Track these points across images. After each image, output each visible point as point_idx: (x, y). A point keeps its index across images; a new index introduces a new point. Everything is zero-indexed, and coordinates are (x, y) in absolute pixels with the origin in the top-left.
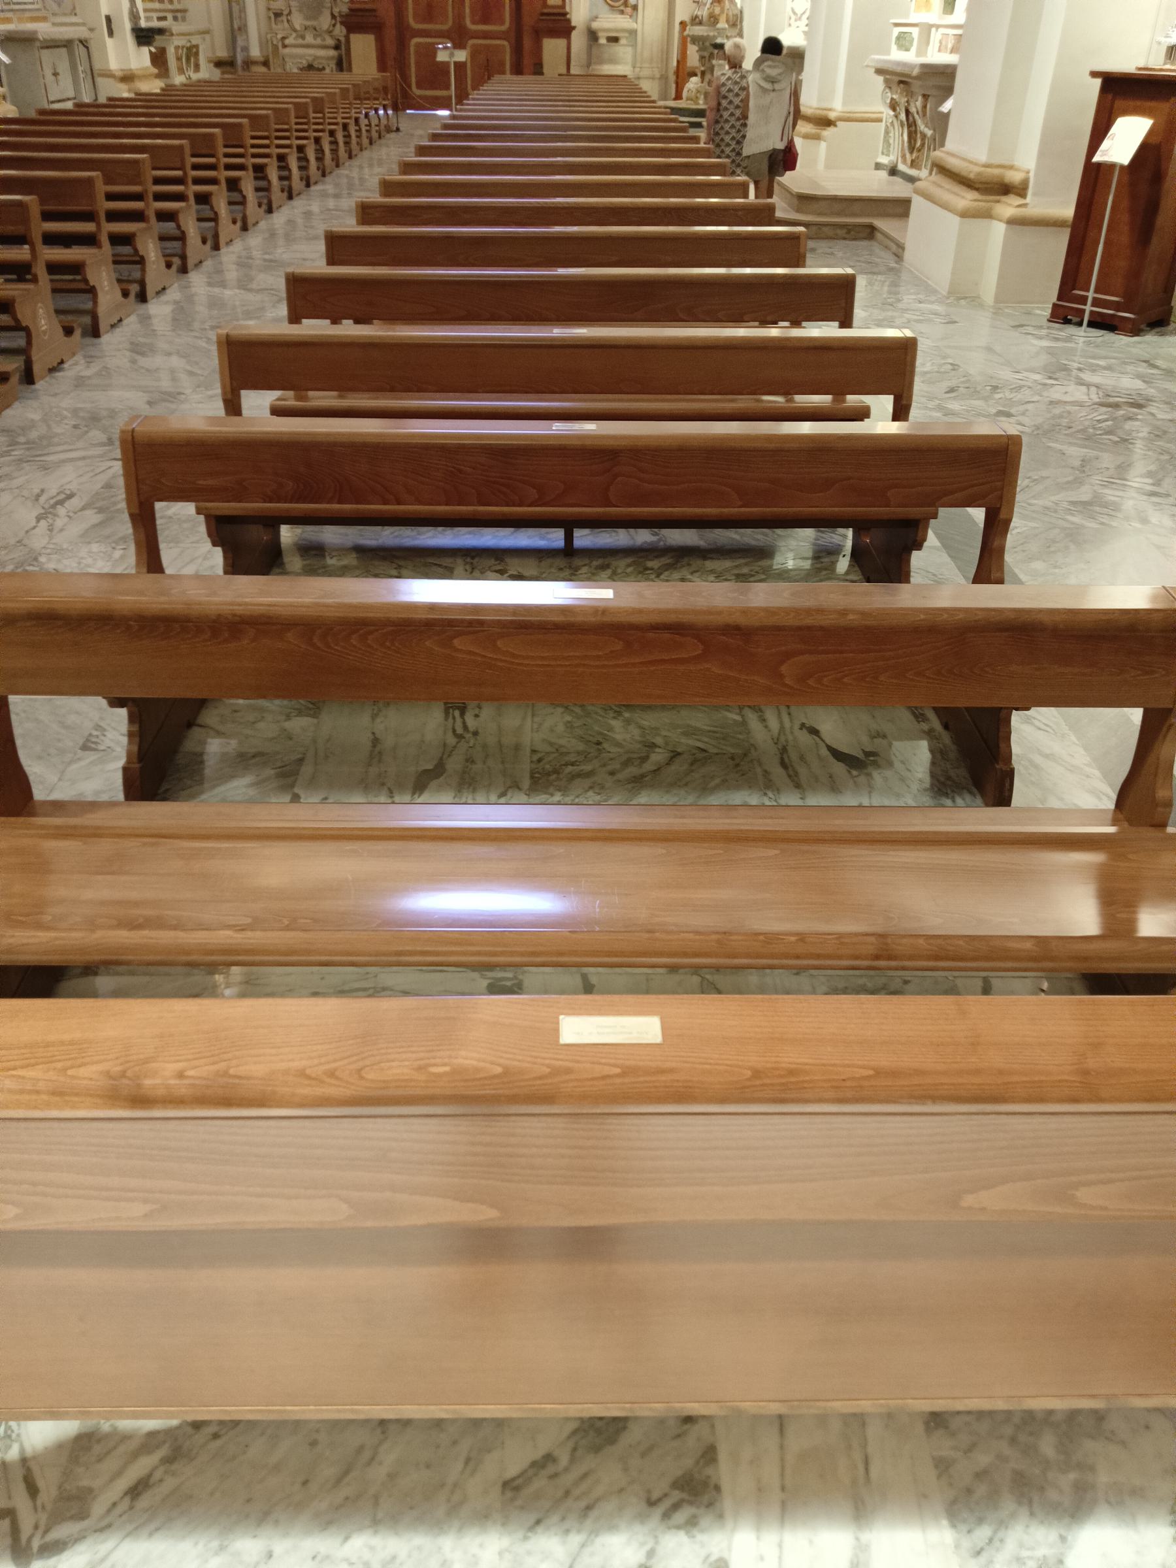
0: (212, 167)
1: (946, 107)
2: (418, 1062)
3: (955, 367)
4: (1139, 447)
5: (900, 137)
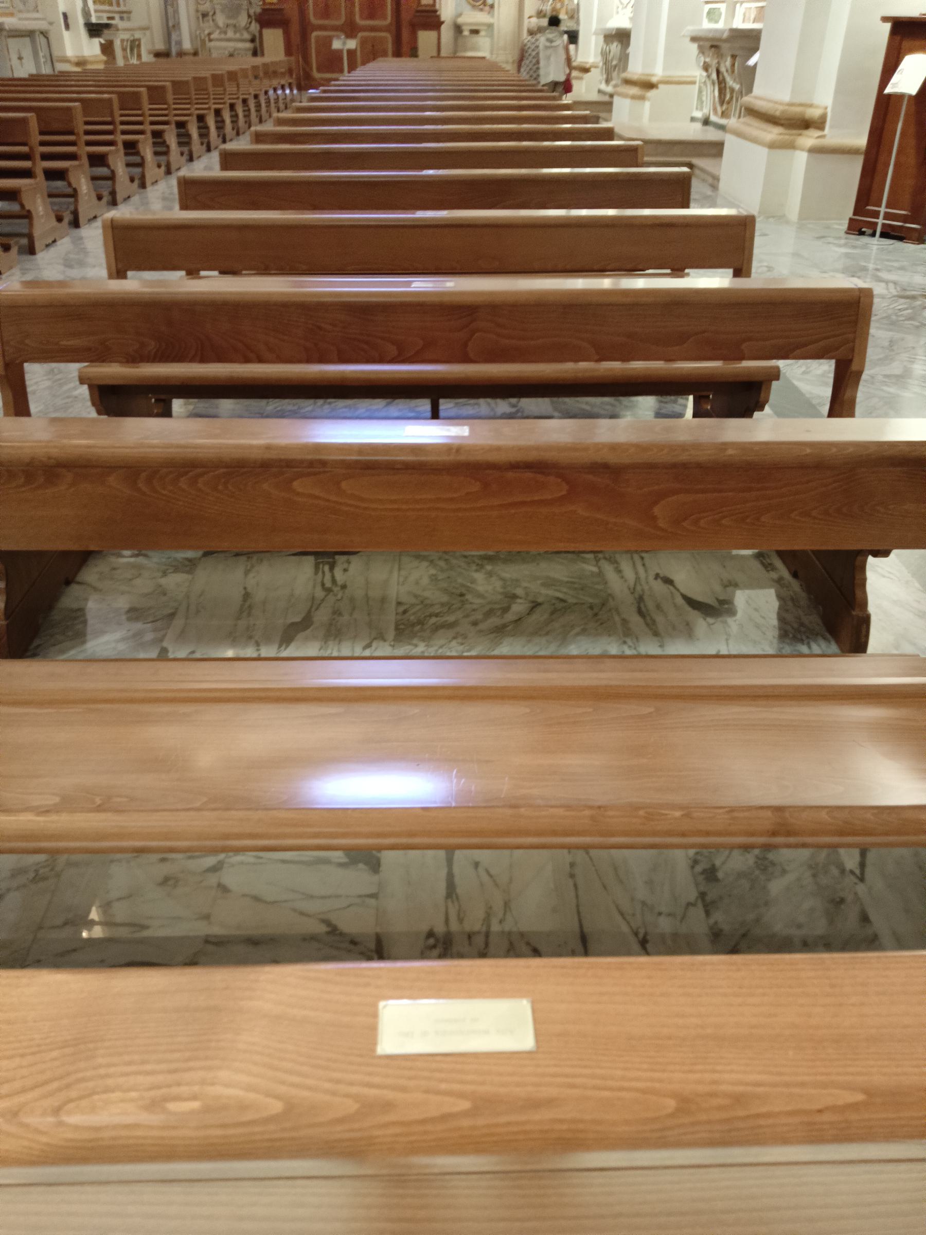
1: (751, 62)
2: (152, 1093)
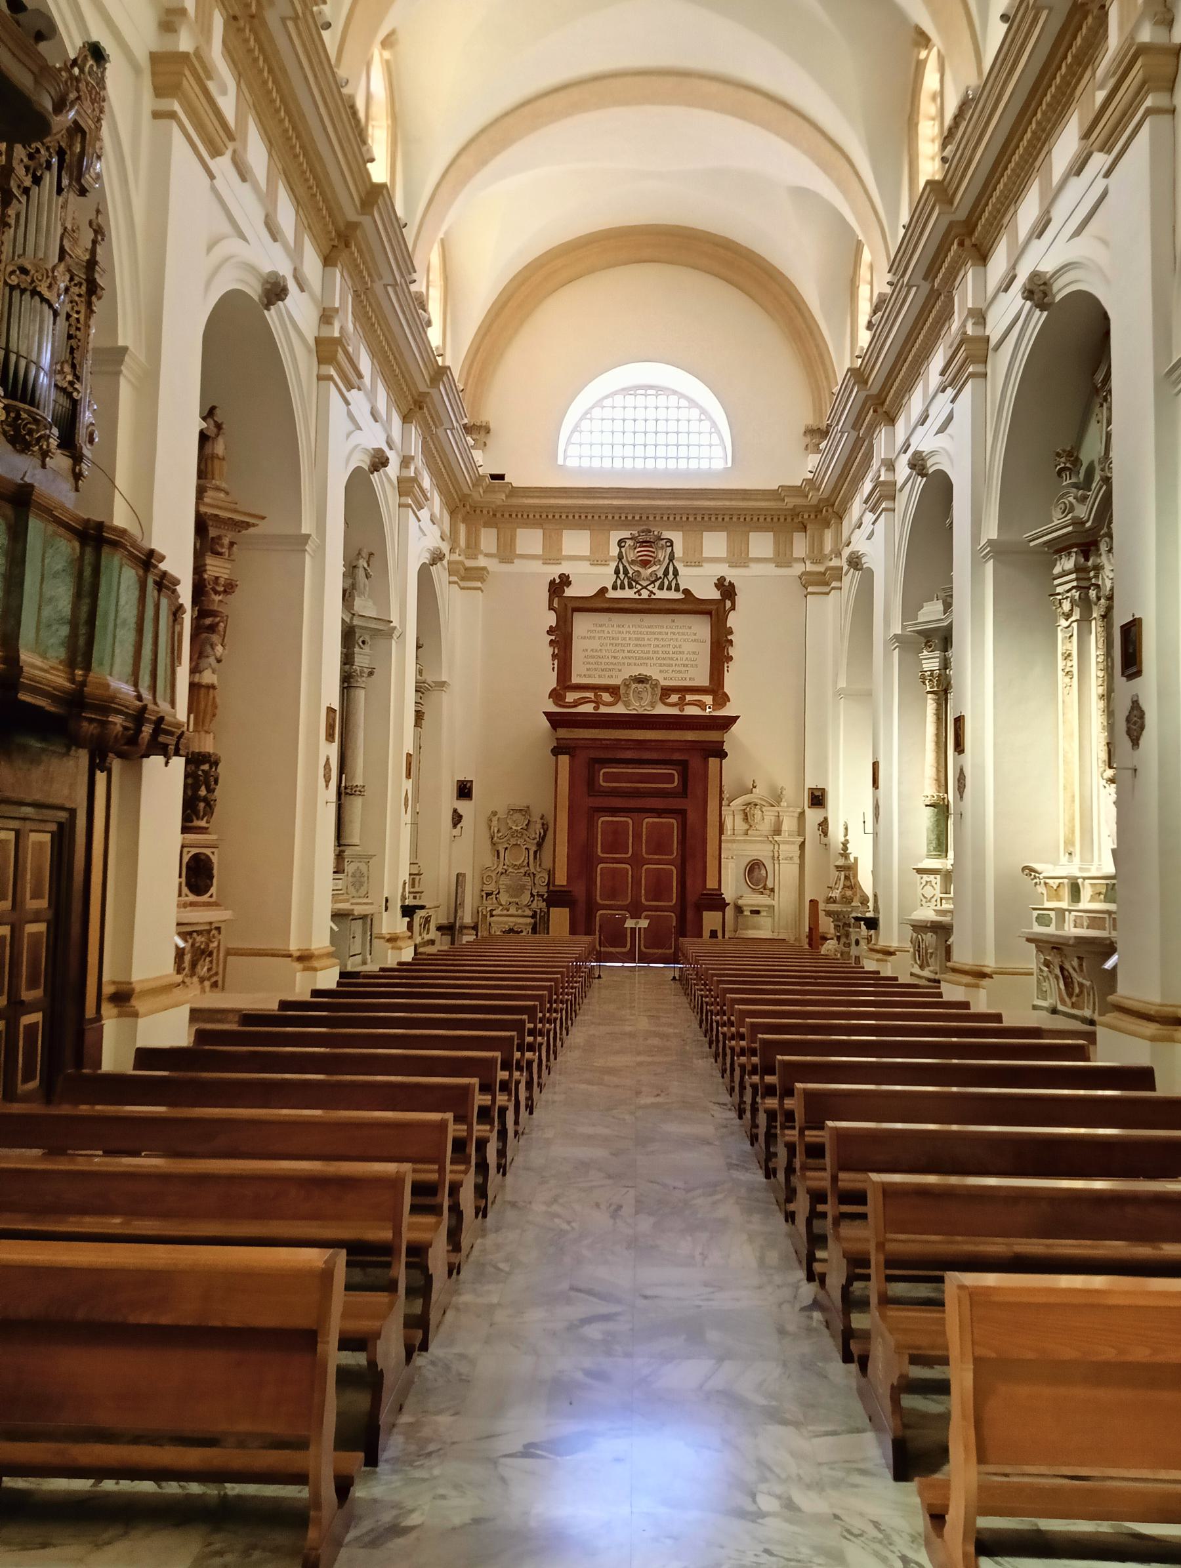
1: (1109, 965)
5: (1054, 987)
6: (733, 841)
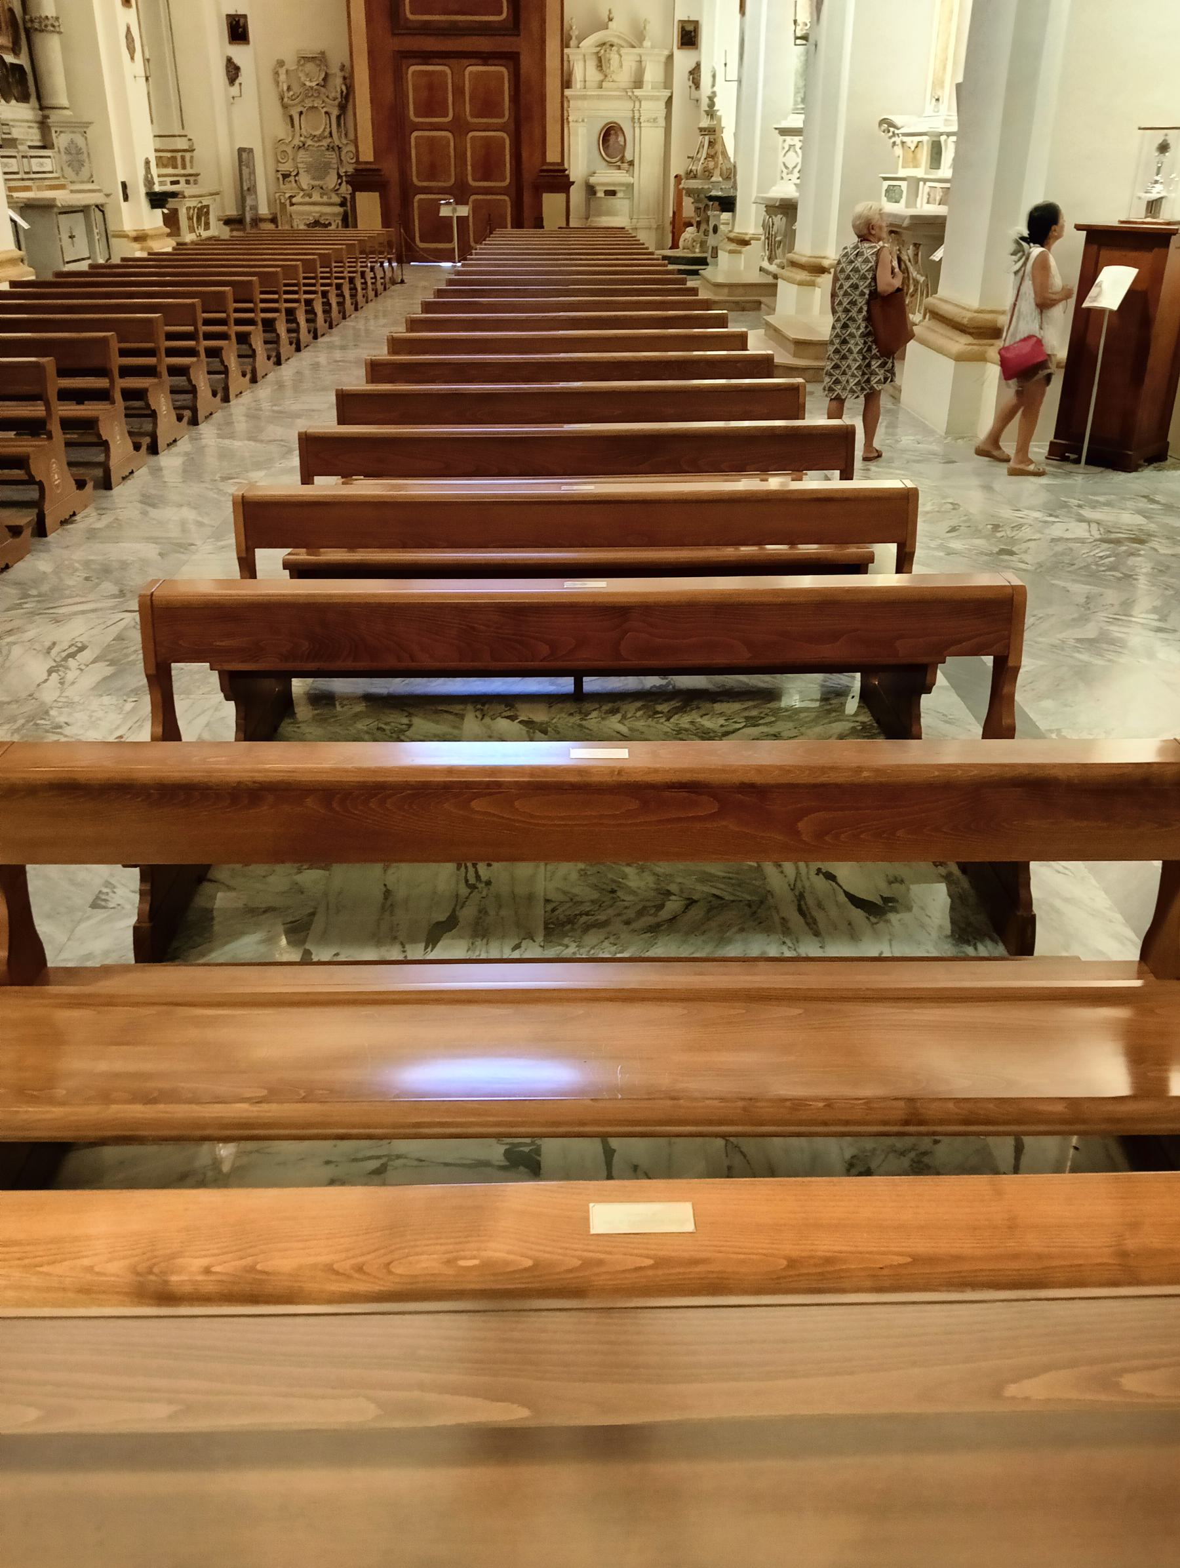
0: (223, 322)
1: (937, 255)
3: (955, 506)
4: (1142, 583)
6: (584, 97)
